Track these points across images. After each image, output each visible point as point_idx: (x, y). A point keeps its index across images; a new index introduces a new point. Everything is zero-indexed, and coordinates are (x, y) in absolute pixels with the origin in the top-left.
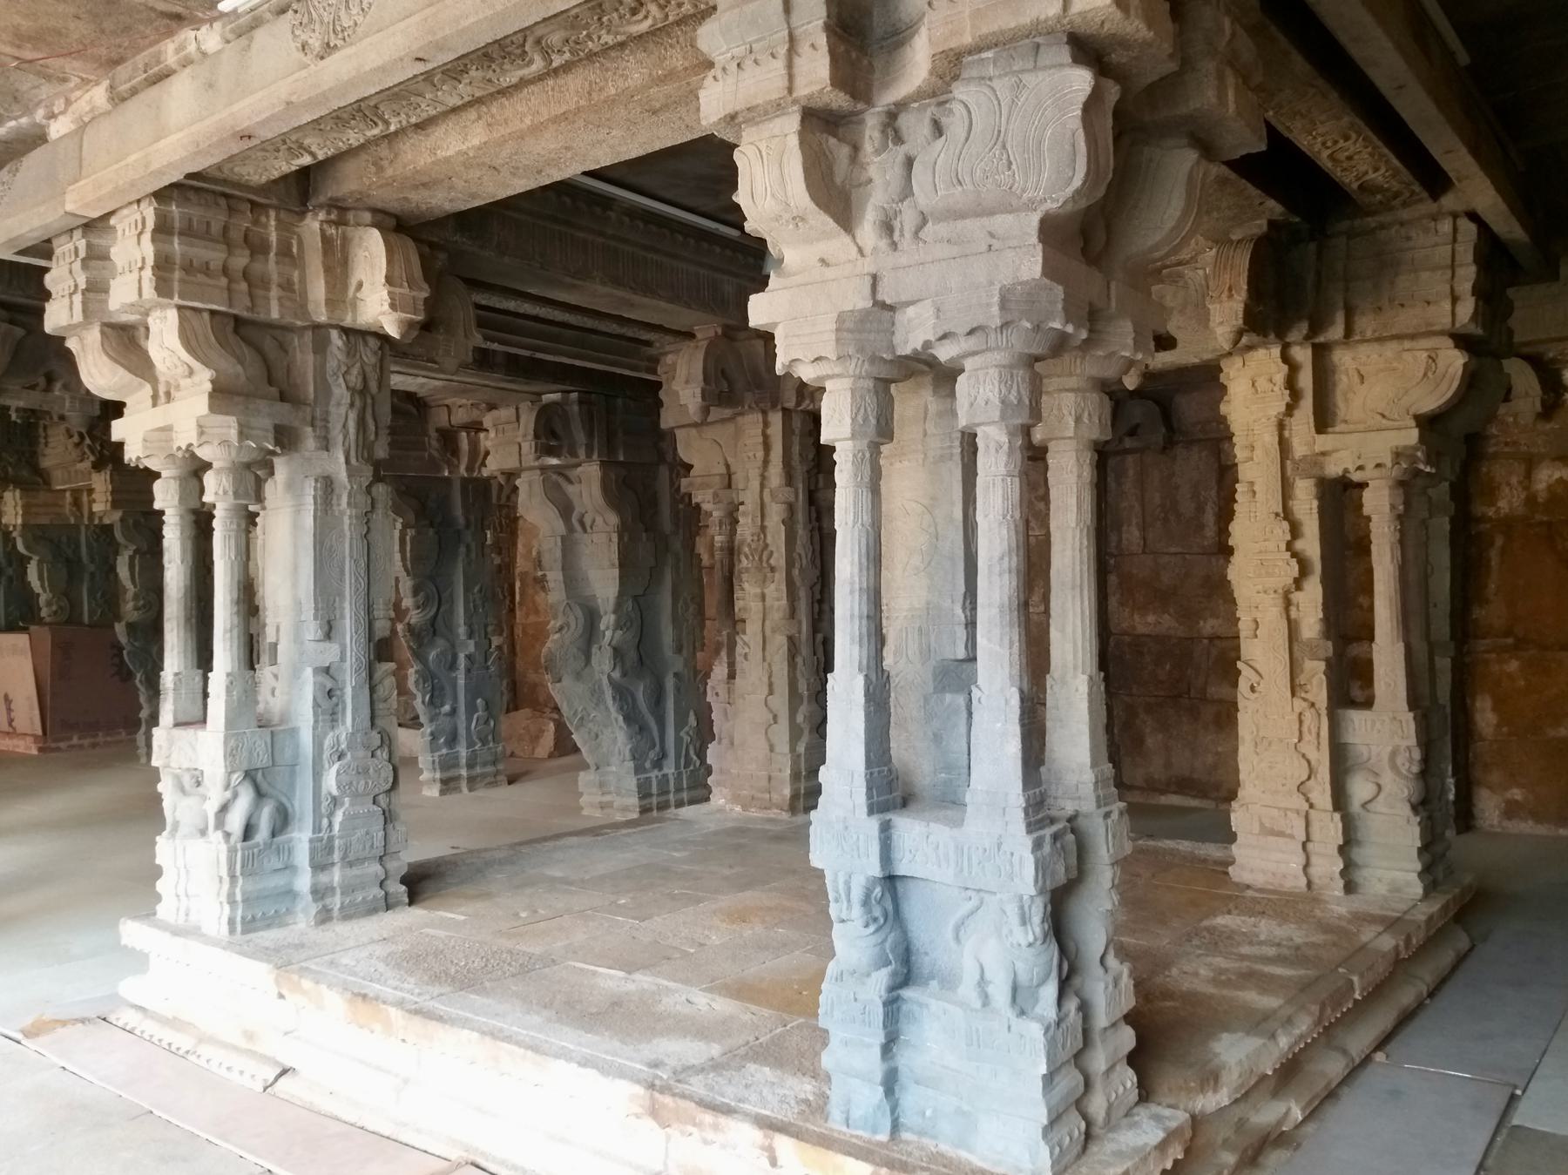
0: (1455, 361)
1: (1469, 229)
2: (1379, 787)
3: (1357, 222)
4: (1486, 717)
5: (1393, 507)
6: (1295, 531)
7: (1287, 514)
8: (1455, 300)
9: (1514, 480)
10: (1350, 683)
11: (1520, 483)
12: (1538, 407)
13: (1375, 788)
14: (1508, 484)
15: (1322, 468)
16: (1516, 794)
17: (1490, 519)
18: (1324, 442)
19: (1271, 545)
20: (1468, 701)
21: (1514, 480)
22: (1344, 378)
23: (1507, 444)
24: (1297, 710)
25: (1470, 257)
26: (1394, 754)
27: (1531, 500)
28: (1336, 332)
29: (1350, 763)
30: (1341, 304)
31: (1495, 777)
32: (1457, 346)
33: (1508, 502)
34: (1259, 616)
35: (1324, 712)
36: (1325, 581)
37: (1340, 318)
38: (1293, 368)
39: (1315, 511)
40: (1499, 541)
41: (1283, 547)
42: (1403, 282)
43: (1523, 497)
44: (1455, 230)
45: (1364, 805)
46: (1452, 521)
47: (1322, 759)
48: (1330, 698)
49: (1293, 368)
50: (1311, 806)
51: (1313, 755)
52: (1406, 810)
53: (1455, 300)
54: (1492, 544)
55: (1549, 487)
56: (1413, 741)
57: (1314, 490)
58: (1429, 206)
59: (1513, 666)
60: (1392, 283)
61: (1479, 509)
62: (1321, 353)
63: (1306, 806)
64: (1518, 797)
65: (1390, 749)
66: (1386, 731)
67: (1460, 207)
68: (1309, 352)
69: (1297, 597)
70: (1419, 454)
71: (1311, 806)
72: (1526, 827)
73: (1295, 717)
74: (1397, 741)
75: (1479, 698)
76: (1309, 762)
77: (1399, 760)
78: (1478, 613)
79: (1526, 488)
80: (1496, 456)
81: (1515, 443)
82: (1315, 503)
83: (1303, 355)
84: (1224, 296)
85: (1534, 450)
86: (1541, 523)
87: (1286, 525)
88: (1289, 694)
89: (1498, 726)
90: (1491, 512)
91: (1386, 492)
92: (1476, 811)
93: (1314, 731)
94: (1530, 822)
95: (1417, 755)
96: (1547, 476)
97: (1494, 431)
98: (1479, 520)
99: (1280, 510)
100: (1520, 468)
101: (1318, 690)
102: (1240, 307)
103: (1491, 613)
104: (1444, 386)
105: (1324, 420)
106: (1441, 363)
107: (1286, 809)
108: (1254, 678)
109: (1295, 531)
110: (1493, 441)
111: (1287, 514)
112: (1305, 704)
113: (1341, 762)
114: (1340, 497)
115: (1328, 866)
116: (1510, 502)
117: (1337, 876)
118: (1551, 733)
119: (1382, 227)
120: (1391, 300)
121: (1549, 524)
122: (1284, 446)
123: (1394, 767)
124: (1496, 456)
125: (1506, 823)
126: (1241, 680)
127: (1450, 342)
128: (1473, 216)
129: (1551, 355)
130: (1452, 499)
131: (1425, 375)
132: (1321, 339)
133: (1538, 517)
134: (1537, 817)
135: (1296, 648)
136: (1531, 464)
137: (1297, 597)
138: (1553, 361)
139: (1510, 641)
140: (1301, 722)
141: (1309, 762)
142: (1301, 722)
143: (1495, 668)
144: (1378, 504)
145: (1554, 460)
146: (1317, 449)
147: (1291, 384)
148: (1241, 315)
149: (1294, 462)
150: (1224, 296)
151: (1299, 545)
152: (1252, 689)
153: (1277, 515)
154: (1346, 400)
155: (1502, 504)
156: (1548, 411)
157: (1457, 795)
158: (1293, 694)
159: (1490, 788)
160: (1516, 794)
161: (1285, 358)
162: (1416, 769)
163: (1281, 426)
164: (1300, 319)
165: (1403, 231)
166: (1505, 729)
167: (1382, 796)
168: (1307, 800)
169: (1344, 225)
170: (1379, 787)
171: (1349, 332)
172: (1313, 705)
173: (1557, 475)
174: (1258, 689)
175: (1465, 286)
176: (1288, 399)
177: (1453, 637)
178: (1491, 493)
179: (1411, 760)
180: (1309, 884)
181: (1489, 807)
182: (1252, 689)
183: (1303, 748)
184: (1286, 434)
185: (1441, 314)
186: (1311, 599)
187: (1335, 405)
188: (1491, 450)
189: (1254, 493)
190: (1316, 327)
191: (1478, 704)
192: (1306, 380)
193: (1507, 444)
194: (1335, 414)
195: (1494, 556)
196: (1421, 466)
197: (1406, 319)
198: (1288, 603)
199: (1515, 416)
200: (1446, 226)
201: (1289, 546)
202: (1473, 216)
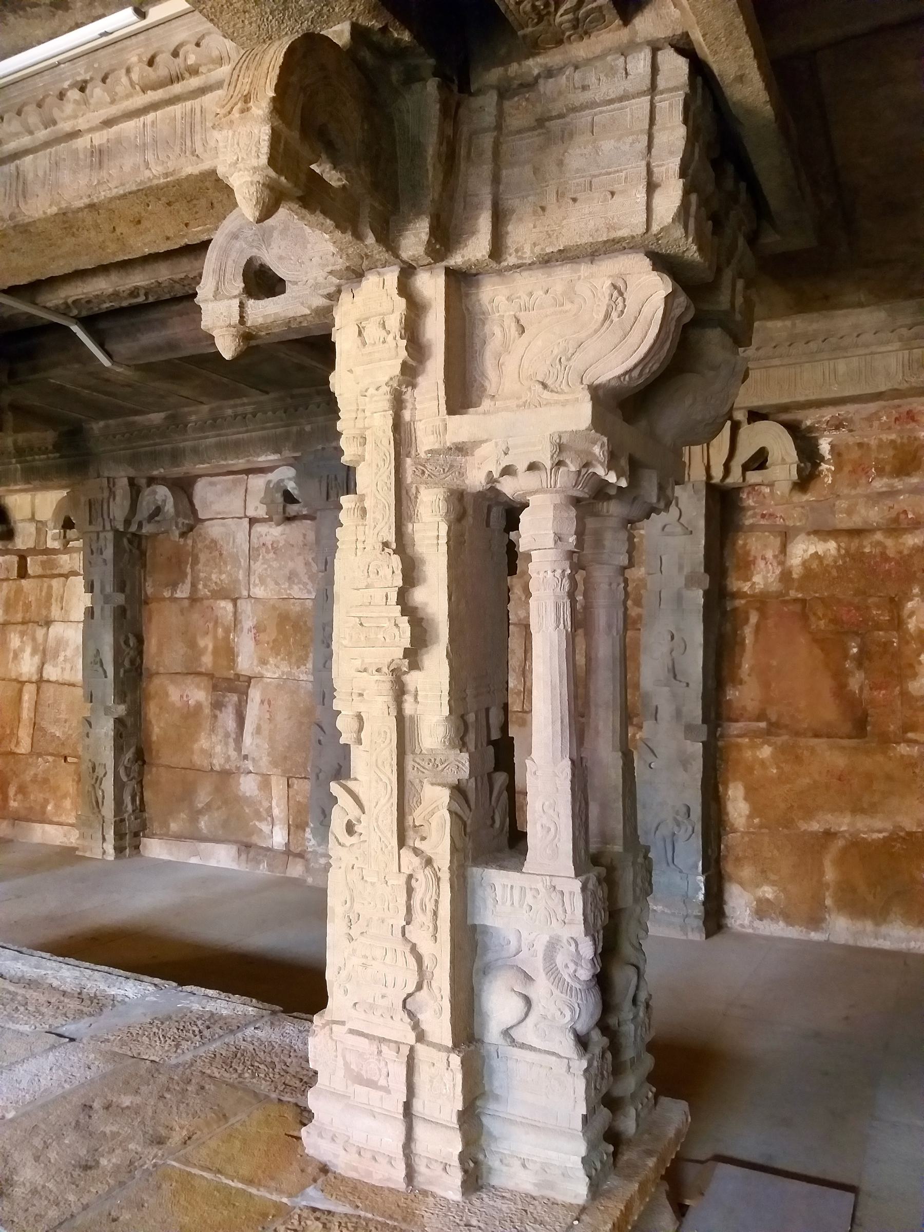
0: (651, 291)
1: (676, 68)
2: (528, 1001)
3: (514, 68)
4: (737, 807)
5: (559, 538)
6: (411, 574)
7: (402, 545)
8: (651, 187)
9: (769, 554)
10: (492, 829)
11: (775, 557)
12: (794, 476)
13: (520, 1004)
14: (764, 558)
15: (461, 474)
16: (768, 892)
17: (744, 595)
18: (462, 427)
19: (378, 595)
20: (721, 788)
21: (769, 554)
22: (497, 331)
23: (763, 516)
24: (406, 870)
25: (678, 116)
26: (552, 947)
27: (785, 576)
28: (475, 249)
29: (490, 956)
30: (488, 203)
31: (747, 872)
32: (655, 268)
33: (763, 578)
34: (363, 708)
35: (445, 876)
36: (453, 655)
37: (484, 223)
38: (415, 309)
39: (444, 540)
40: (754, 618)
41: (393, 597)
42: (577, 157)
43: (778, 571)
44: (655, 69)
45: (506, 1033)
46: (706, 594)
47: (439, 953)
48: (454, 849)
49: (415, 309)
50: (421, 1037)
51: (426, 948)
52: (567, 1046)
53: (651, 187)
54: (747, 620)
55: (804, 563)
56: (578, 929)
57: (443, 506)
58: (623, 35)
59: (766, 752)
60: (560, 163)
61: (735, 584)
62: (461, 282)
63: (411, 1038)
64: (770, 896)
65: (545, 939)
66: (538, 909)
67: (662, 33)
68: (441, 280)
69: (413, 679)
70: (597, 450)
71: (421, 1037)
72: (776, 929)
73: (403, 880)
74: (557, 928)
75: (731, 785)
76: (419, 959)
77: (561, 959)
78: (732, 694)
79: (782, 563)
80: (752, 528)
81: (771, 515)
82: (444, 528)
83: (431, 285)
84: (236, 114)
85: (790, 523)
86: (796, 600)
87: (396, 560)
88: (395, 842)
89: (750, 817)
90: (746, 587)
91: (550, 514)
92: (727, 909)
93: (430, 906)
94: (782, 924)
95: (587, 949)
96: (802, 550)
97: (751, 502)
98: (735, 595)
99: (391, 538)
100: (776, 542)
101: (438, 841)
102: (264, 133)
103: (744, 694)
104: (634, 337)
105: (461, 394)
106: (632, 298)
107: (382, 1040)
108: (353, 811)
109: (411, 574)
110: (750, 513)
111: (402, 545)
112: (416, 861)
113: (470, 950)
114: (487, 526)
115: (441, 1145)
116: (765, 578)
117: (456, 1162)
118: (804, 826)
119: (550, 73)
120: (560, 195)
121: (803, 601)
122: (400, 429)
123: (552, 970)
124: (752, 528)
125: (757, 923)
126: (335, 811)
127: (647, 262)
128: (684, 47)
129: (808, 423)
130: (707, 570)
131: (607, 316)
132: (456, 260)
133: (793, 594)
134: (789, 919)
135: (409, 763)
136: (786, 537)
137: (413, 679)
138: (810, 429)
139: (763, 725)
140: (410, 891)
141: (419, 959)
142: (410, 891)
143: (748, 754)
144: (541, 534)
145: (809, 534)
146: (451, 439)
147: (412, 332)
148: (265, 148)
149: (418, 462)
150: (236, 114)
151: (419, 596)
152: (350, 829)
153: (386, 545)
154: (499, 365)
155: (757, 579)
156: (805, 480)
157: (707, 895)
158: (402, 843)
159: (741, 884)
160: (768, 892)
161: (405, 289)
162: (585, 973)
163: (398, 403)
164: (418, 215)
165: (577, 75)
166: (756, 821)
167: (530, 1020)
168: (416, 1026)
169: (494, 75)
170: (528, 1001)
171: (497, 251)
172: (429, 862)
173: (812, 550)
174: (358, 828)
175: (669, 165)
176: (404, 354)
177: (705, 720)
178: (746, 567)
179: (577, 958)
180: (410, 1175)
181: (740, 905)
182: (350, 829)
183: (414, 934)
184: (407, 415)
185: (627, 213)
186: (433, 680)
187: (483, 374)
188: (748, 522)
189: (364, 511)
190: (444, 239)
191: (730, 793)
192: (435, 328)
193: (763, 516)
194: (483, 389)
195: (748, 633)
196: (600, 471)
197: (578, 223)
198: (400, 691)
199: (771, 485)
200: (640, 63)
201: (403, 596)
202: (684, 47)
